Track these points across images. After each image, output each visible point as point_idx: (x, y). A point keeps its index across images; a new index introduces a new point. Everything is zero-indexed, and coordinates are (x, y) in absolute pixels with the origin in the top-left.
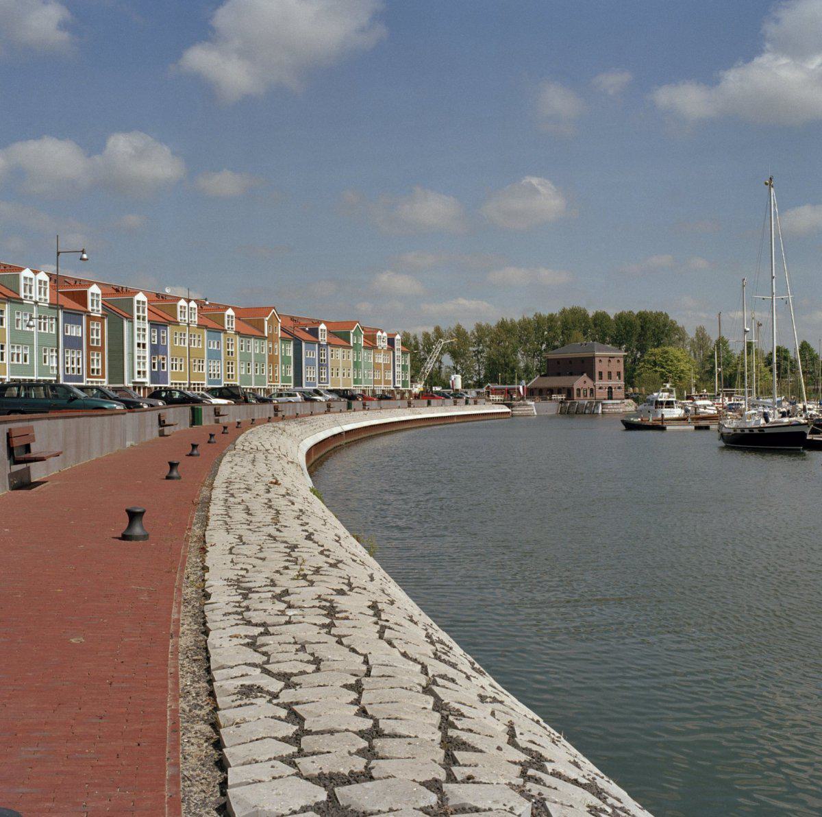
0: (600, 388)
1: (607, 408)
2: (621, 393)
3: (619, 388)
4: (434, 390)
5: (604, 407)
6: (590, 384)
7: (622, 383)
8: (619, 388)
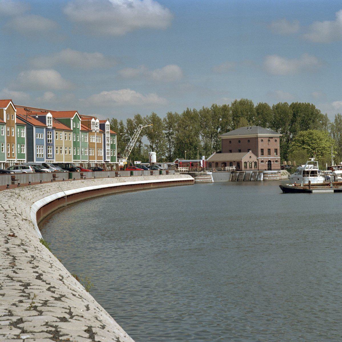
0: (262, 162)
1: (267, 177)
2: (277, 165)
3: (276, 161)
4: (135, 163)
5: (265, 175)
6: (254, 158)
7: (278, 158)
8: (276, 161)
